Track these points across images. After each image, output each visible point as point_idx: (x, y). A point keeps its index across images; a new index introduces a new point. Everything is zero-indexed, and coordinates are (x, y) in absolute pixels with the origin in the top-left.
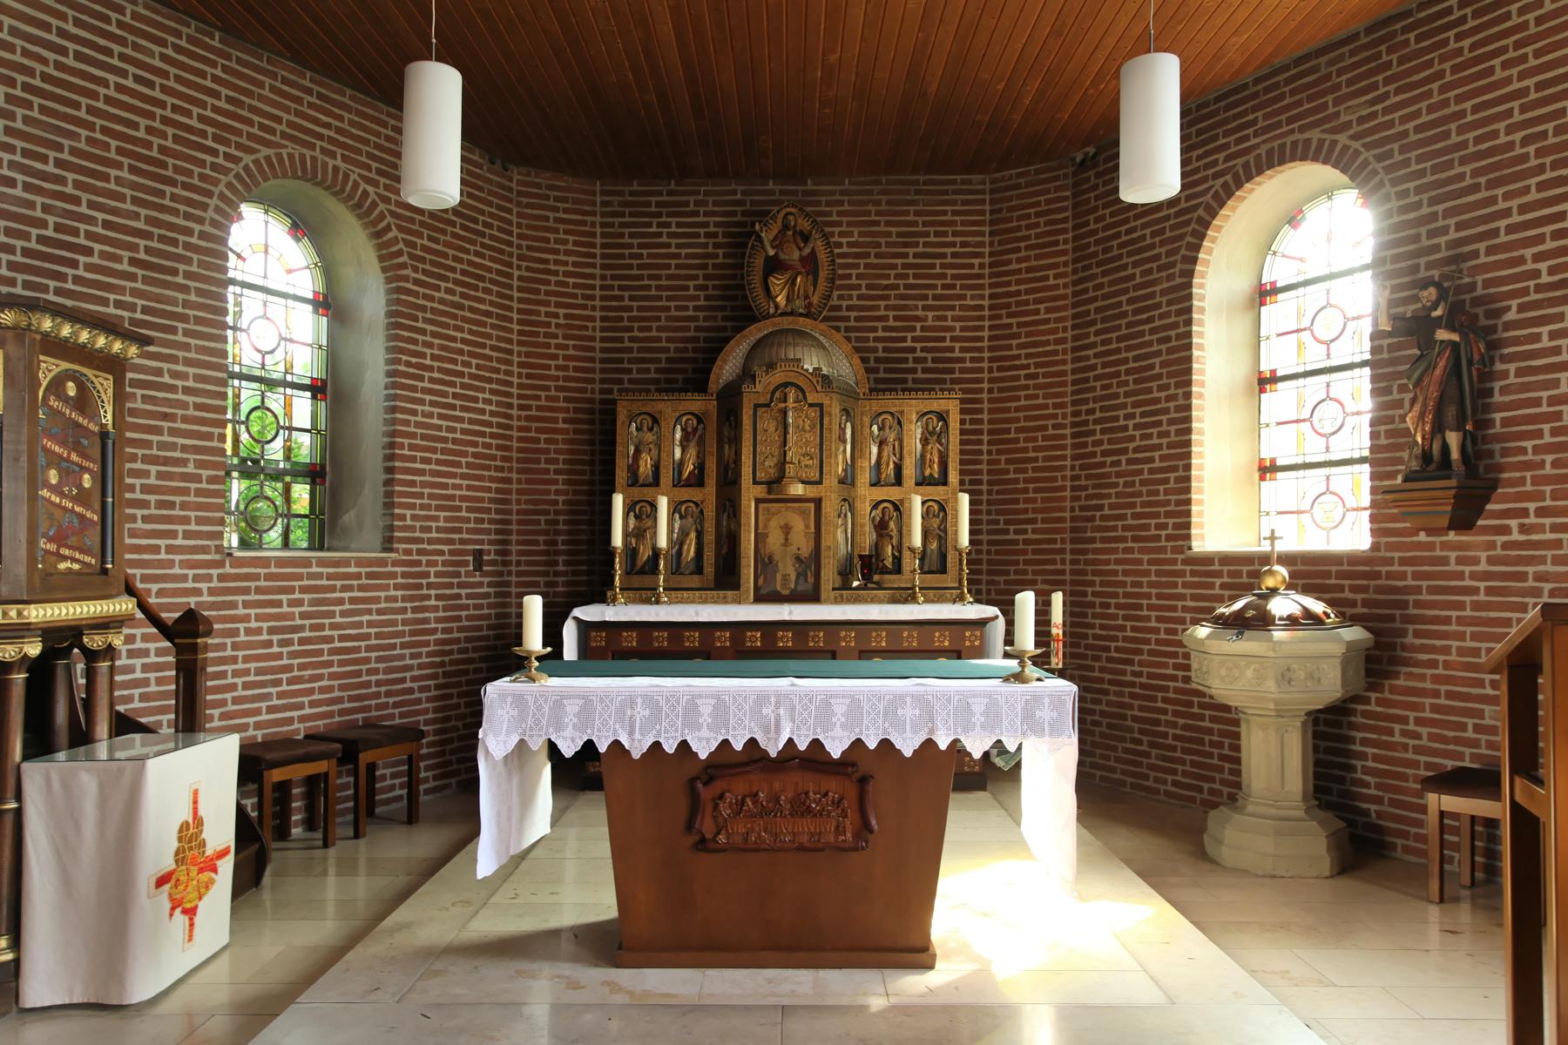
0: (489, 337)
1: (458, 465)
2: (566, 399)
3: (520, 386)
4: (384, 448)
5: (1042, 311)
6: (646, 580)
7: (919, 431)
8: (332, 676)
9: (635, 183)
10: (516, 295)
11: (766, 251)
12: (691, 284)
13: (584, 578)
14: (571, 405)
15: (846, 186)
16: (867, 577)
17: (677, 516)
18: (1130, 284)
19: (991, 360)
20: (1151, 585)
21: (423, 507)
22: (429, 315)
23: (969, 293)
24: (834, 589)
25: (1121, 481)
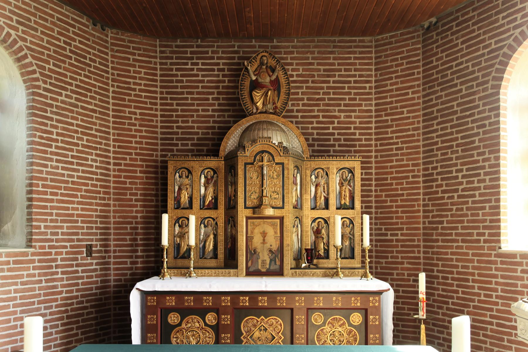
0: (95, 124)
2: (141, 160)
3: (114, 152)
4: (26, 187)
5: (405, 112)
7: (338, 179)
9: (179, 41)
10: (111, 101)
11: (251, 77)
12: (211, 97)
13: (153, 259)
14: (144, 164)
15: (295, 43)
16: (310, 261)
17: (202, 226)
18: (459, 95)
19: (376, 140)
20: (474, 268)
21: (52, 221)
22: (54, 110)
23: (364, 103)
24: (291, 269)
25: (454, 208)
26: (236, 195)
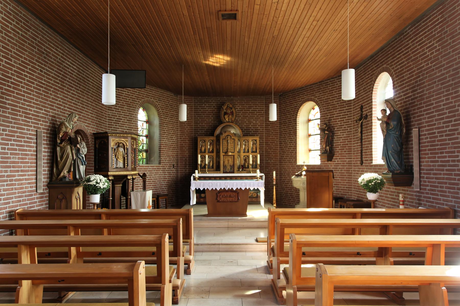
0: (175, 126)
1: (170, 149)
2: (188, 137)
3: (180, 135)
6: (204, 169)
8: (153, 185)
15: (239, 98)
19: (265, 130)
26: (220, 149)
